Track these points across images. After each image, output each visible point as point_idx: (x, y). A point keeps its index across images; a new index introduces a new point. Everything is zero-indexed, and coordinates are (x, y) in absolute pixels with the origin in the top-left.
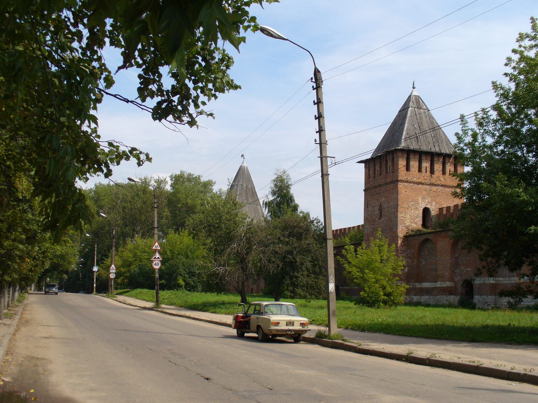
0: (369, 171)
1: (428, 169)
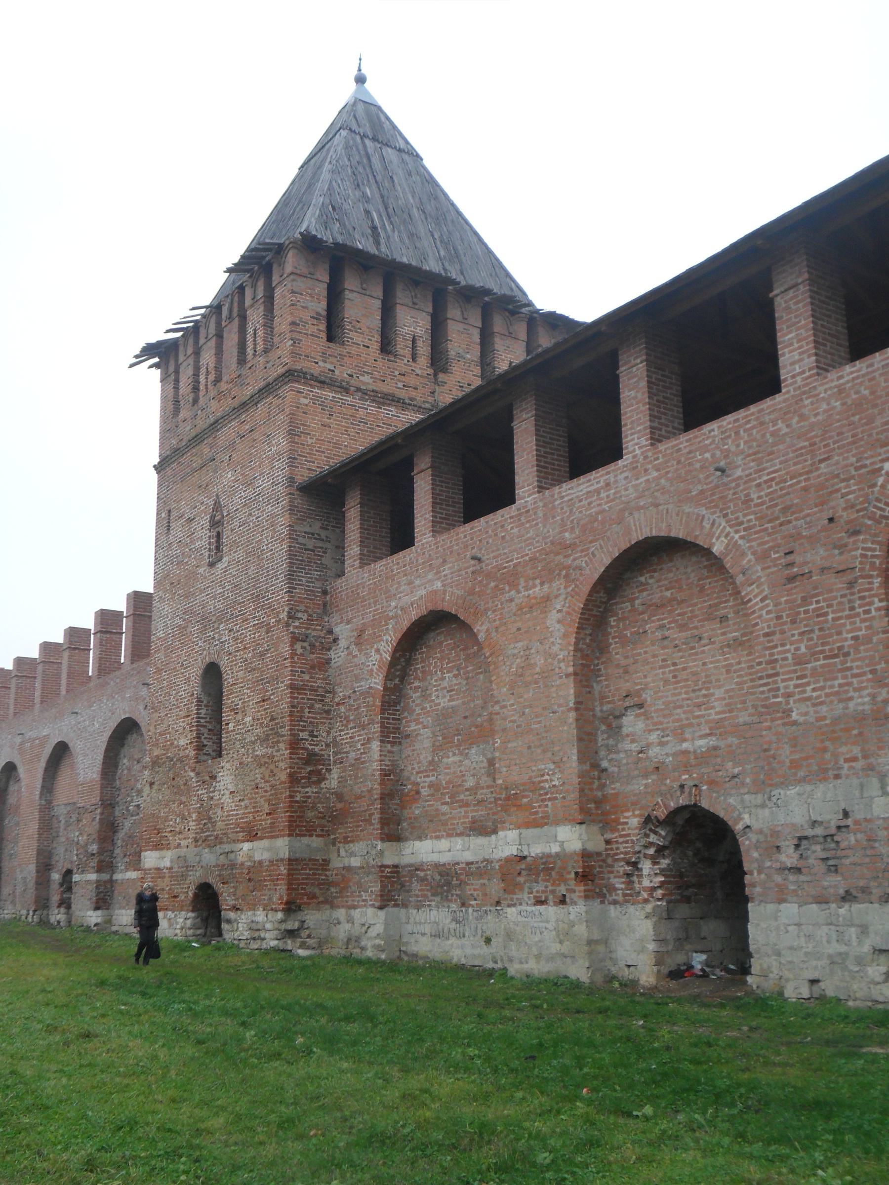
0: (176, 388)
1: (424, 349)
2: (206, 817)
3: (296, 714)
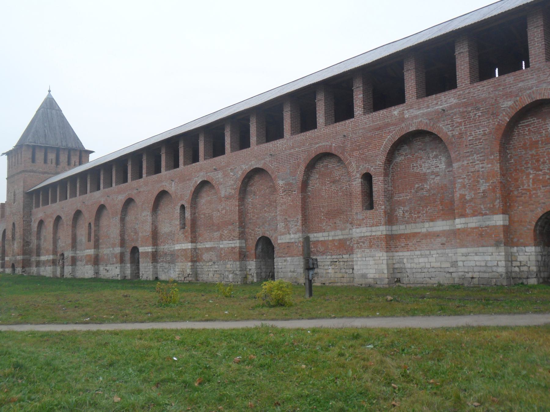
1: (54, 161)
2: (13, 252)
3: (24, 235)
